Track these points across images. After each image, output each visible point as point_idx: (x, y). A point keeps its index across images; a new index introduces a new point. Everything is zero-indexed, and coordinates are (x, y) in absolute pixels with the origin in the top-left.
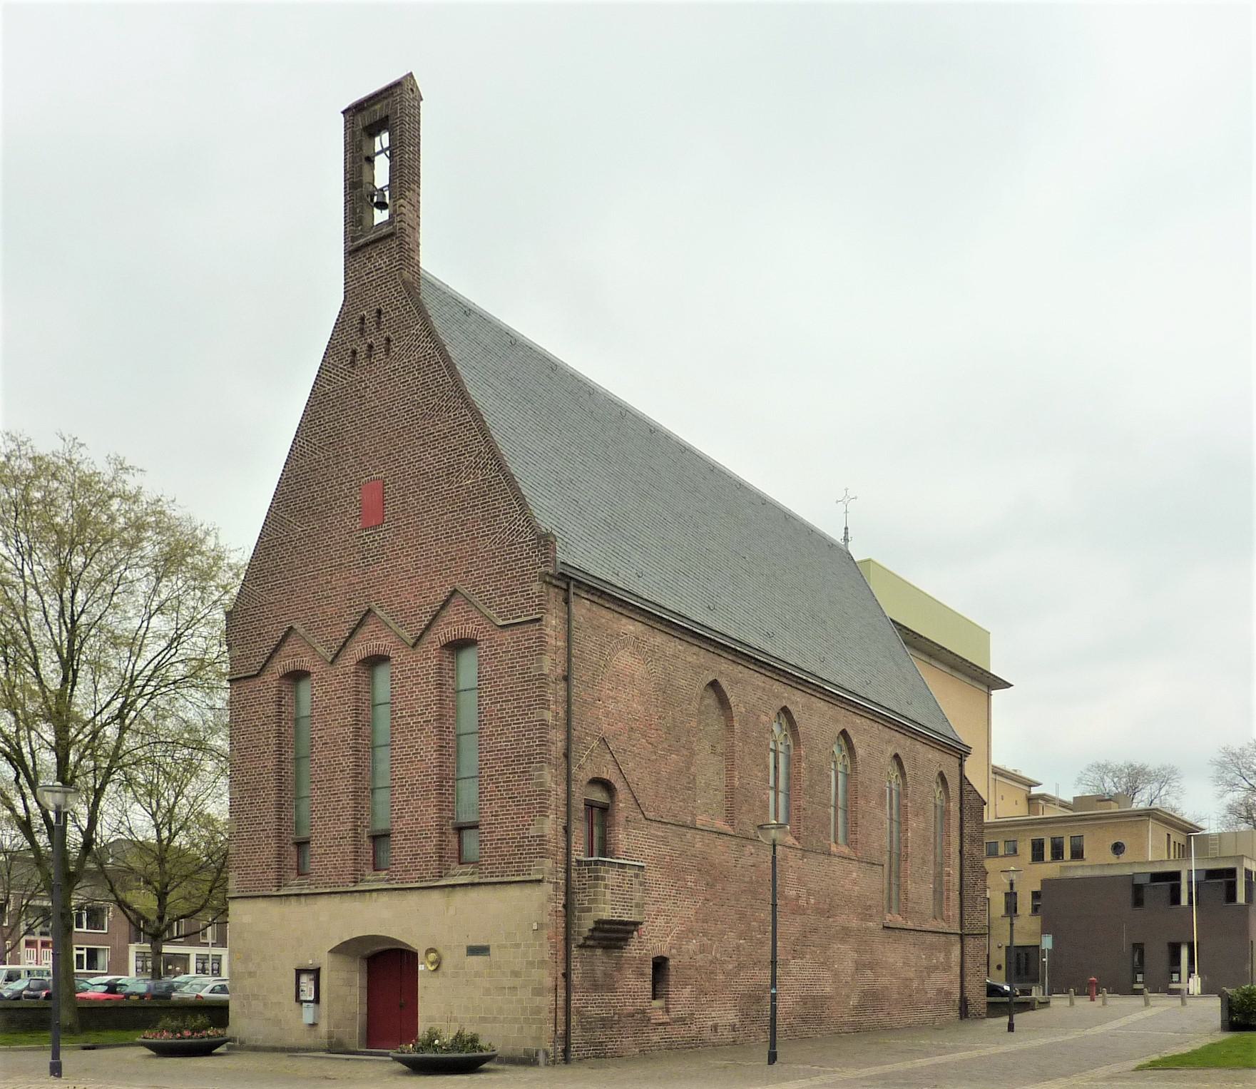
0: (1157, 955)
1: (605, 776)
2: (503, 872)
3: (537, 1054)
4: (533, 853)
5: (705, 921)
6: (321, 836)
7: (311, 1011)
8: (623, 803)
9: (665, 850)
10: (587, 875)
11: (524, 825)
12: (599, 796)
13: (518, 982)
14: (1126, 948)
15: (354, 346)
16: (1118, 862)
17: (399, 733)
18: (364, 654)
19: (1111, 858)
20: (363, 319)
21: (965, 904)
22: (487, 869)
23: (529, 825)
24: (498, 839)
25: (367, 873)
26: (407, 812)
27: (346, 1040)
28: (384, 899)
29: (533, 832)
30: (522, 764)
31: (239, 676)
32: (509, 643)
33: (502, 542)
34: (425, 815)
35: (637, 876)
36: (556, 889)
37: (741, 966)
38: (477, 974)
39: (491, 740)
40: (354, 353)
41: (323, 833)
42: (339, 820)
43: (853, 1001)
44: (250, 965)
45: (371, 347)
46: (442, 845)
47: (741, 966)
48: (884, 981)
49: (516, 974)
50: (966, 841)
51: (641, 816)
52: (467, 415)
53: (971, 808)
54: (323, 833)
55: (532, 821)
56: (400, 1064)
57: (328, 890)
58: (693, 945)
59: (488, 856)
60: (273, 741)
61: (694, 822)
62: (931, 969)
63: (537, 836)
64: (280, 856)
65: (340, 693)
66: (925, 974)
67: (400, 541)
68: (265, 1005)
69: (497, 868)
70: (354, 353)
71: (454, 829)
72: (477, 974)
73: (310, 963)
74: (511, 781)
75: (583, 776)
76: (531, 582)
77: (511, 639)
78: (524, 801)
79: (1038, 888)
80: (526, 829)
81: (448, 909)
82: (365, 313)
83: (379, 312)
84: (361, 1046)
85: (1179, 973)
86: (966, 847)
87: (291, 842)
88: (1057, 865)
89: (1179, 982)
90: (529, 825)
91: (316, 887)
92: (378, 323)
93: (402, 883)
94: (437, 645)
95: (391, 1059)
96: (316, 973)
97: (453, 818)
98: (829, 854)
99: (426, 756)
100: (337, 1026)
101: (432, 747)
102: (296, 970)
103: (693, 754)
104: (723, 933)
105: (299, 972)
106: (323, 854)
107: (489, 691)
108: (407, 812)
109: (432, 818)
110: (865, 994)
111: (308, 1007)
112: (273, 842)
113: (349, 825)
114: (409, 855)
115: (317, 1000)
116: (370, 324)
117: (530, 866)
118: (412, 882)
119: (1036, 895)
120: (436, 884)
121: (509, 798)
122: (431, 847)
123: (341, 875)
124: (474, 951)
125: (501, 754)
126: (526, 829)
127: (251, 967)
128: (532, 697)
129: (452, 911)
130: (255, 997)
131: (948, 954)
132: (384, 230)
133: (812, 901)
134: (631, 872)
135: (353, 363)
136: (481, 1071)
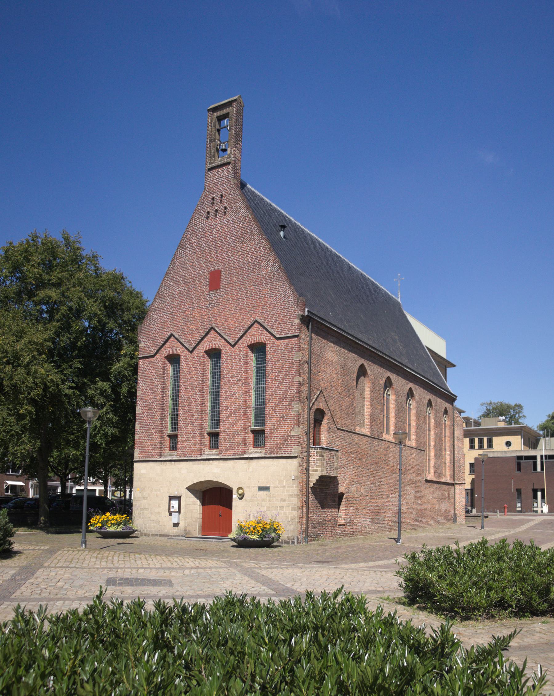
0: (527, 493)
1: (321, 408)
2: (278, 452)
3: (294, 539)
4: (293, 444)
5: (358, 476)
6: (183, 433)
7: (177, 517)
9: (343, 443)
10: (315, 454)
11: (288, 430)
13: (284, 504)
14: (513, 490)
15: (209, 210)
16: (508, 450)
17: (225, 385)
18: (208, 348)
19: (505, 448)
20: (213, 199)
21: (456, 469)
22: (269, 450)
24: (275, 437)
25: (206, 450)
26: (228, 422)
27: (192, 531)
30: (288, 401)
31: (144, 356)
32: (282, 346)
33: (279, 299)
34: (237, 424)
35: (335, 455)
36: (302, 461)
37: (371, 498)
38: (263, 500)
39: (272, 390)
40: (208, 213)
41: (185, 431)
42: (193, 425)
43: (414, 515)
44: (144, 494)
45: (217, 211)
46: (245, 438)
47: (371, 498)
48: (425, 505)
49: (283, 500)
50: (456, 439)
51: (335, 427)
52: (263, 243)
53: (458, 424)
54: (185, 431)
55: (293, 428)
56: (233, 542)
57: (187, 458)
58: (353, 488)
59: (269, 444)
60: (160, 387)
61: (355, 429)
62: (443, 500)
63: (295, 436)
64: (161, 442)
65: (195, 365)
66: (440, 502)
67: (228, 297)
68: (152, 514)
69: (274, 450)
70: (208, 213)
71: (251, 431)
72: (263, 500)
73: (175, 493)
74: (282, 409)
76: (294, 318)
77: (283, 344)
78: (288, 419)
79: (473, 461)
80: (290, 432)
81: (249, 469)
82: (215, 195)
83: (222, 196)
84: (198, 535)
85: (537, 503)
86: (456, 442)
87: (167, 435)
88: (481, 452)
89: (537, 507)
91: (180, 457)
92: (221, 201)
93: (225, 456)
94: (246, 345)
95: (230, 540)
96: (179, 498)
98: (405, 446)
99: (239, 396)
100: (189, 525)
101: (242, 392)
102: (169, 497)
103: (354, 398)
104: (365, 482)
106: (184, 441)
107: (272, 367)
108: (228, 422)
109: (241, 426)
110: (418, 512)
112: (158, 435)
113: (199, 428)
114: (229, 443)
115: (179, 512)
116: (217, 201)
117: (291, 449)
118: (230, 455)
119: (472, 465)
120: (241, 457)
121: (281, 417)
122: (240, 439)
123: (194, 451)
124: (261, 489)
125: (277, 396)
126: (290, 432)
127: (145, 495)
128: (293, 370)
129: (251, 470)
130: (147, 509)
131: (449, 492)
132: (225, 160)
134: (334, 453)
135: (208, 218)
136: (273, 547)
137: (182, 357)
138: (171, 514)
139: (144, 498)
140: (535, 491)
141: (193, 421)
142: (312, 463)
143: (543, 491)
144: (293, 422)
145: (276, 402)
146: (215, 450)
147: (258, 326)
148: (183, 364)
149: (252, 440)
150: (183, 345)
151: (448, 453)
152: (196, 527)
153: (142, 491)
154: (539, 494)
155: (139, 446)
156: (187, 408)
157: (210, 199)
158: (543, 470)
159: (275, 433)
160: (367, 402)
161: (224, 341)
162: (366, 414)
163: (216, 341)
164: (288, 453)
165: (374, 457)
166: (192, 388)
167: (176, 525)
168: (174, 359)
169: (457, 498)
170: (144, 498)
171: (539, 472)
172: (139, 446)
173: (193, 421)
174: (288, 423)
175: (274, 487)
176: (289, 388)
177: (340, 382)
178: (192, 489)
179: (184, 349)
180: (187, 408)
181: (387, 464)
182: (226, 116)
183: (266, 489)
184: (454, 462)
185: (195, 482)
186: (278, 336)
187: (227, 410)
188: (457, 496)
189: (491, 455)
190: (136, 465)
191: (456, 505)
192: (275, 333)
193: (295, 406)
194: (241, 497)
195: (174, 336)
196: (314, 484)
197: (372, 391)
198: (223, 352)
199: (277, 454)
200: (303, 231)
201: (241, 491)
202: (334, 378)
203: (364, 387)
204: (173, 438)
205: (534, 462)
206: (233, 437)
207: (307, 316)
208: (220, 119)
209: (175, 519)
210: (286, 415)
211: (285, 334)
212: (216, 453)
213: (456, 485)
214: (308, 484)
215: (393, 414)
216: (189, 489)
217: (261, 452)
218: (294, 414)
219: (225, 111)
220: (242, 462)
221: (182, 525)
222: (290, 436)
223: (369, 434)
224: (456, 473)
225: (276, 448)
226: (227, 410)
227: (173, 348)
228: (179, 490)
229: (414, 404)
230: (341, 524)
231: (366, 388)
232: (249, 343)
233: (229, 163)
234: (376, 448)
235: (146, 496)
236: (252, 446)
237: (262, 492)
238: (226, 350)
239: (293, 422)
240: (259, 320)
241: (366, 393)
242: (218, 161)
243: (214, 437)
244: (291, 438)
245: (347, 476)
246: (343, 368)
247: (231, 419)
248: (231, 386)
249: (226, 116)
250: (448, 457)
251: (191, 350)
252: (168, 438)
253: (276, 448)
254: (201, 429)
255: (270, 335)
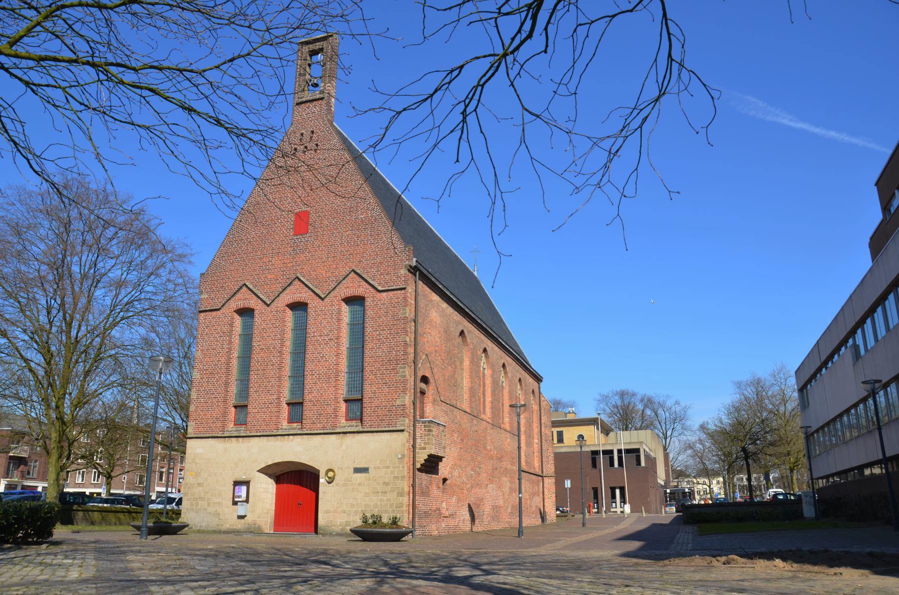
8: (430, 391)
12: (423, 385)
18: (291, 301)
22: (368, 423)
23: (396, 399)
25: (284, 424)
28: (298, 439)
29: (398, 402)
37: (472, 487)
38: (360, 484)
47: (472, 487)
49: (386, 484)
51: (439, 399)
55: (398, 396)
63: (401, 405)
67: (317, 243)
75: (420, 374)
81: (341, 445)
85: (616, 503)
86: (543, 429)
89: (616, 507)
90: (396, 399)
91: (251, 432)
96: (247, 483)
97: (343, 394)
100: (259, 517)
105: (237, 483)
109: (332, 394)
111: (242, 505)
113: (275, 397)
115: (247, 501)
124: (357, 470)
127: (200, 480)
129: (344, 447)
130: (202, 499)
133: (495, 453)
134: (441, 428)
137: (256, 312)
138: (235, 503)
139: (199, 485)
140: (613, 490)
141: (269, 387)
142: (419, 440)
143: (622, 490)
144: (400, 389)
145: (377, 365)
146: (296, 424)
147: (355, 276)
148: (257, 319)
149: (345, 411)
150: (259, 297)
151: (536, 441)
152: (268, 521)
153: (197, 475)
154: (618, 492)
155: (195, 419)
156: (261, 372)
157: (298, 135)
158: (622, 466)
159: (376, 402)
160: (466, 374)
161: (311, 293)
162: (465, 388)
163: (301, 293)
164: (392, 427)
165: (474, 438)
166: (268, 348)
167: (241, 517)
168: (246, 312)
169: (546, 493)
170: (199, 485)
171: (616, 468)
172: (195, 419)
173: (269, 387)
174: (392, 390)
175: (375, 468)
176: (394, 349)
177: (443, 348)
178: (266, 471)
179: (260, 301)
180: (261, 372)
181: (485, 448)
182: (321, 50)
183: (365, 470)
184: (541, 452)
185: (270, 463)
186: (380, 288)
187: (314, 375)
188: (546, 490)
189: (563, 450)
190: (190, 443)
191: (546, 501)
192: (376, 285)
193: (401, 370)
194: (330, 481)
195: (247, 286)
196: (421, 464)
197: (471, 362)
198: (310, 306)
199: (378, 427)
200: (389, 185)
201: (331, 474)
202: (437, 342)
203: (463, 356)
204: (241, 407)
205: (610, 457)
206: (321, 407)
207: (415, 266)
208: (313, 53)
209: (241, 510)
210: (390, 381)
211: (388, 287)
212: (298, 427)
213: (545, 478)
214: (414, 464)
215: (490, 391)
216: (263, 471)
217: (357, 426)
218: (400, 380)
219: (317, 46)
220: (333, 437)
221: (249, 519)
222: (395, 406)
223: (469, 412)
224: (544, 465)
225: (376, 420)
226: (314, 375)
227: (244, 300)
228: (248, 473)
229: (507, 382)
230: (445, 515)
231: (465, 358)
232: (343, 296)
233: (322, 99)
234: (476, 428)
235: (202, 481)
236: (344, 418)
237: (359, 475)
238: (314, 304)
239: (400, 389)
240: (356, 269)
241: (465, 364)
242: (307, 96)
243: (296, 406)
244: (396, 408)
245: (450, 458)
246: (446, 332)
247: (319, 385)
248: (320, 347)
249: (321, 50)
250: (536, 446)
251: (268, 303)
252: (233, 409)
253: (376, 420)
254: (278, 398)
255: (370, 288)
